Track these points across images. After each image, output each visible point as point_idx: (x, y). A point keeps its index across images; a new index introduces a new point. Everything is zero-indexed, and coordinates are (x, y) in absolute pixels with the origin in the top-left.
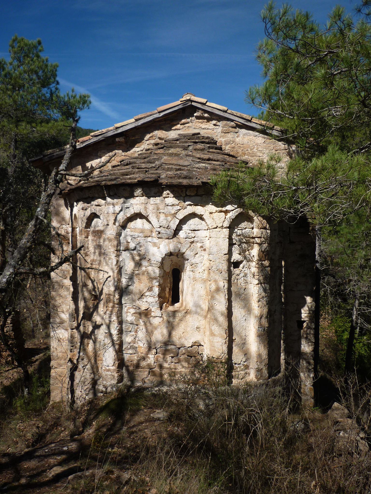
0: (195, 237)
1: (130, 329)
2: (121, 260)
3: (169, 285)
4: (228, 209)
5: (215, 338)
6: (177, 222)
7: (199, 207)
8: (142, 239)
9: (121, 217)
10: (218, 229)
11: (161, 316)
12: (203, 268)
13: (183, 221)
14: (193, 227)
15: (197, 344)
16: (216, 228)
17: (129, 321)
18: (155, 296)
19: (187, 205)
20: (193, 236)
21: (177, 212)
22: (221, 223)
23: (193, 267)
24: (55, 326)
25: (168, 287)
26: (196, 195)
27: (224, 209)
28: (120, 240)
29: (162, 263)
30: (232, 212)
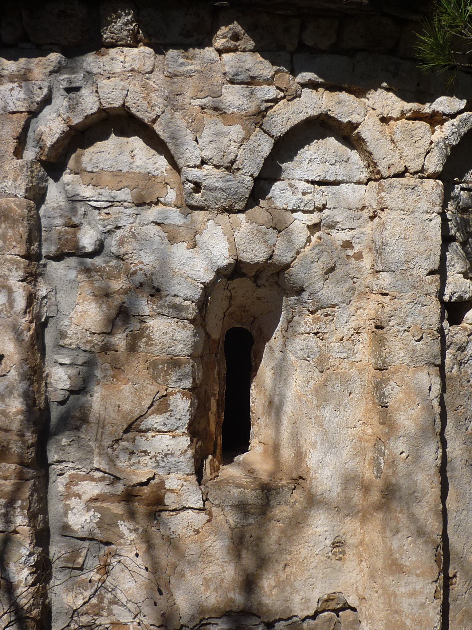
0: (325, 206)
1: (80, 560)
2: (43, 291)
3: (217, 389)
4: (441, 109)
5: (405, 578)
6: (266, 147)
7: (344, 95)
8: (128, 211)
9: (51, 126)
10: (408, 180)
11: (200, 504)
12: (353, 323)
13: (287, 146)
14: (317, 172)
15: (333, 605)
16: (400, 175)
17: (76, 528)
18: (179, 432)
19: (304, 85)
20: (319, 204)
21: (268, 109)
22: (418, 156)
23: (318, 319)
24: (250, 605)
25: (214, 395)
26: (335, 50)
27: (427, 109)
28: (38, 218)
29: (203, 304)
30: (451, 121)
